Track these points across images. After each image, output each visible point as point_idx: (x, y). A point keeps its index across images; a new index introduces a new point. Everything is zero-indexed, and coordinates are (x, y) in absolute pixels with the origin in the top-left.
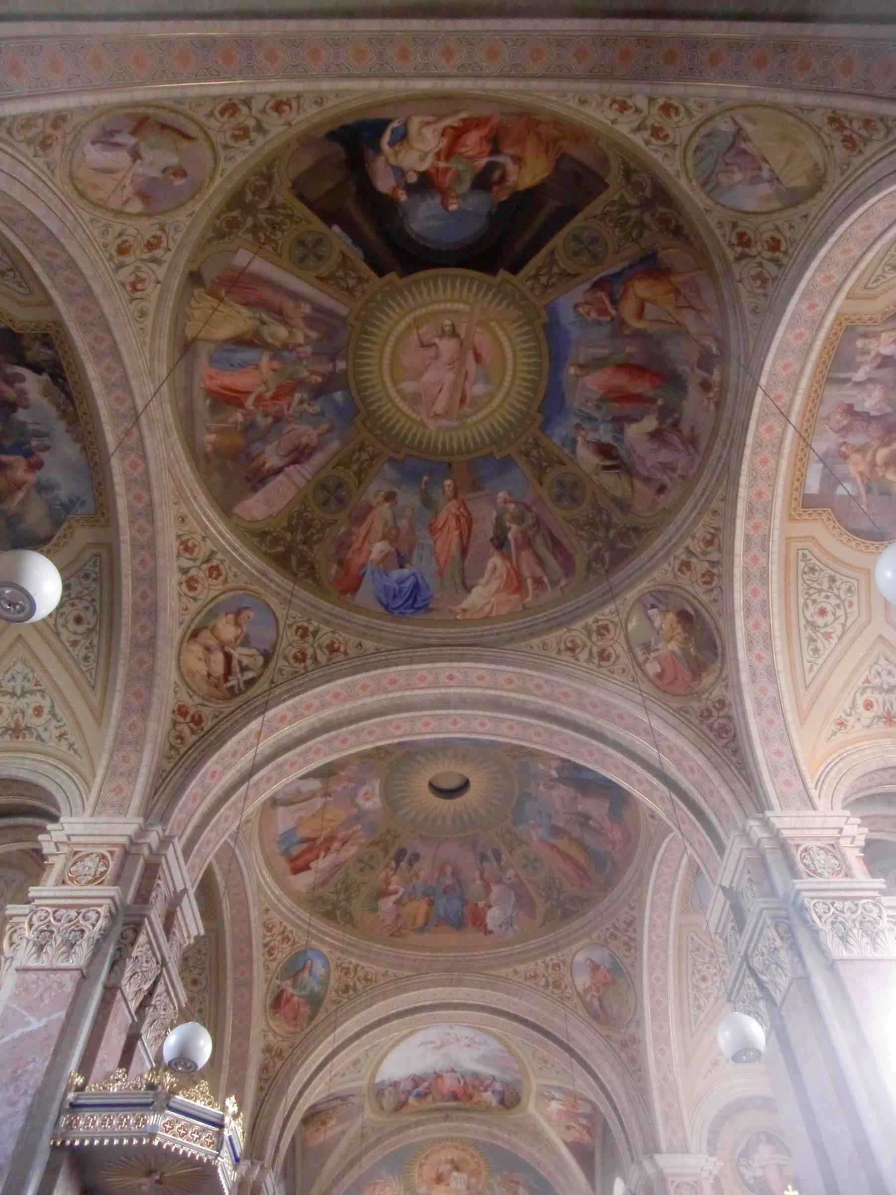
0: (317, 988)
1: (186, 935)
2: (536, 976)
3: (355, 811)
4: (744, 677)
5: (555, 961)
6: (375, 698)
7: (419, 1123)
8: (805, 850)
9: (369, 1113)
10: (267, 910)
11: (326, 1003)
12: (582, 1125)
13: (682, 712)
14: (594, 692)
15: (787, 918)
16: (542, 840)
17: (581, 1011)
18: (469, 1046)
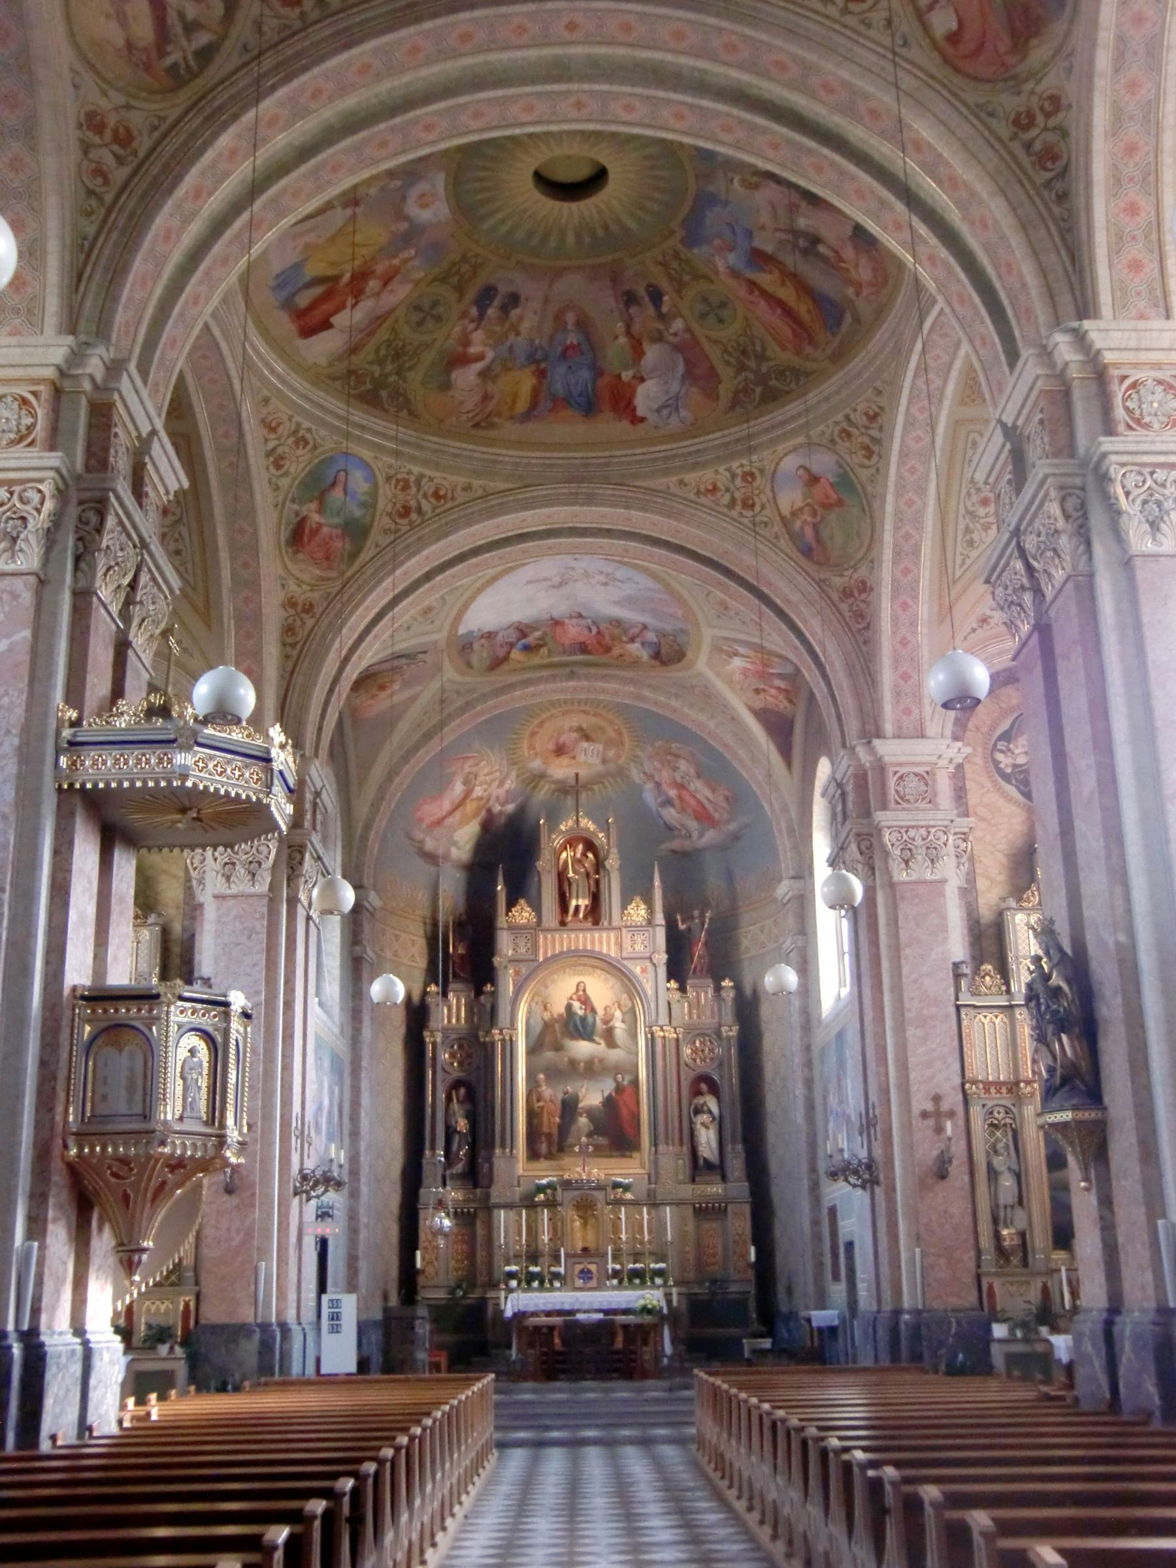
0: (358, 513)
1: (162, 492)
2: (715, 489)
3: (404, 226)
4: (1103, 60)
5: (747, 469)
6: (436, 69)
7: (527, 683)
8: (1134, 385)
9: (450, 673)
10: (266, 401)
11: (375, 536)
12: (779, 689)
13: (982, 113)
14: (829, 66)
15: (1083, 489)
16: (734, 273)
17: (785, 543)
18: (606, 584)
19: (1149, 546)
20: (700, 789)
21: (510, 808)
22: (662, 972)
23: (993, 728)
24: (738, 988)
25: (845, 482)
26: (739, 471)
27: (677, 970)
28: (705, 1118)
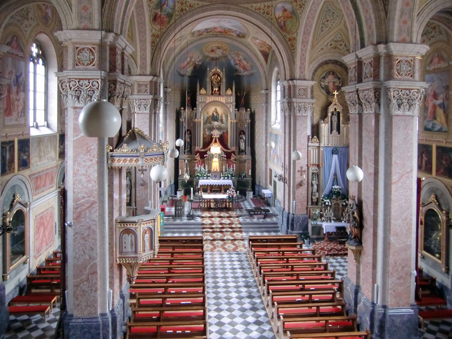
0: (170, 11)
2: (260, 9)
19: (398, 113)
20: (245, 63)
21: (200, 63)
22: (234, 107)
23: (321, 75)
24: (251, 111)
25: (293, 13)
26: (267, 5)
27: (238, 106)
28: (242, 140)
